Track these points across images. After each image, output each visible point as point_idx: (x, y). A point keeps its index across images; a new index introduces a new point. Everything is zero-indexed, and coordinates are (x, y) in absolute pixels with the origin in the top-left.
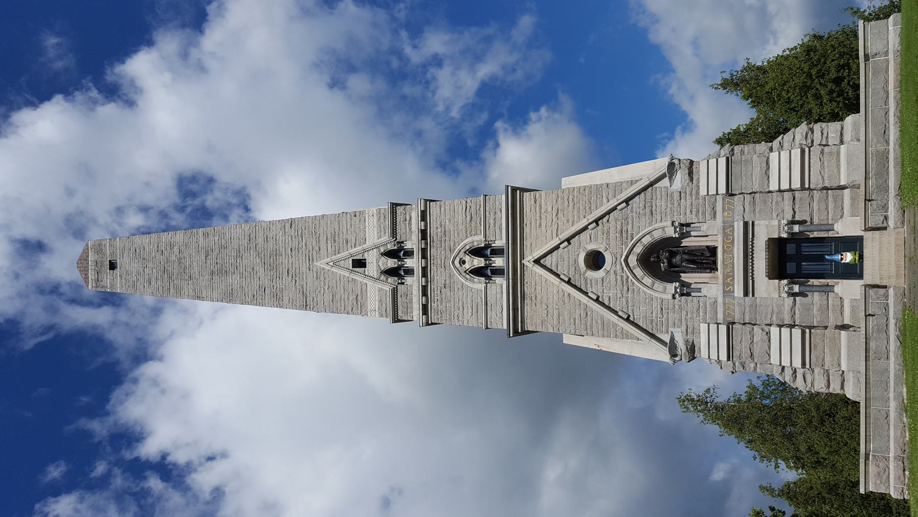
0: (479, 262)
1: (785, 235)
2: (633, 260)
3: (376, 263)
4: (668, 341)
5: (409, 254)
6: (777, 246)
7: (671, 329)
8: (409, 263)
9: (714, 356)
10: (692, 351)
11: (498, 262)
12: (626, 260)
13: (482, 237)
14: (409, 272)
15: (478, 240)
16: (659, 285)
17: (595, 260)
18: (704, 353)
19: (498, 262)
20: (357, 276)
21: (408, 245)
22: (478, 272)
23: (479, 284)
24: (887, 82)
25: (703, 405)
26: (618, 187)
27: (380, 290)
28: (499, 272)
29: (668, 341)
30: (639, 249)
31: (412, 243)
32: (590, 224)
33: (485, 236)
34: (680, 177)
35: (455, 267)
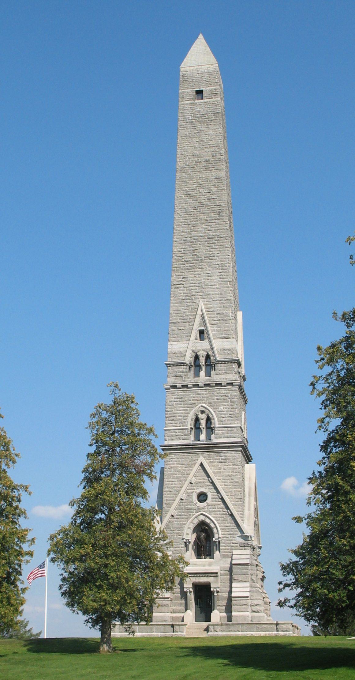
1: (212, 589)
3: (202, 347)
5: (208, 374)
6: (207, 586)
11: (203, 437)
12: (202, 514)
13: (217, 426)
14: (197, 375)
15: (216, 423)
19: (203, 437)
20: (195, 333)
23: (190, 423)
26: (242, 513)
27: (313, 626)
28: (197, 438)
30: (208, 521)
31: (216, 377)
32: (230, 511)
33: (217, 428)
34: (241, 540)
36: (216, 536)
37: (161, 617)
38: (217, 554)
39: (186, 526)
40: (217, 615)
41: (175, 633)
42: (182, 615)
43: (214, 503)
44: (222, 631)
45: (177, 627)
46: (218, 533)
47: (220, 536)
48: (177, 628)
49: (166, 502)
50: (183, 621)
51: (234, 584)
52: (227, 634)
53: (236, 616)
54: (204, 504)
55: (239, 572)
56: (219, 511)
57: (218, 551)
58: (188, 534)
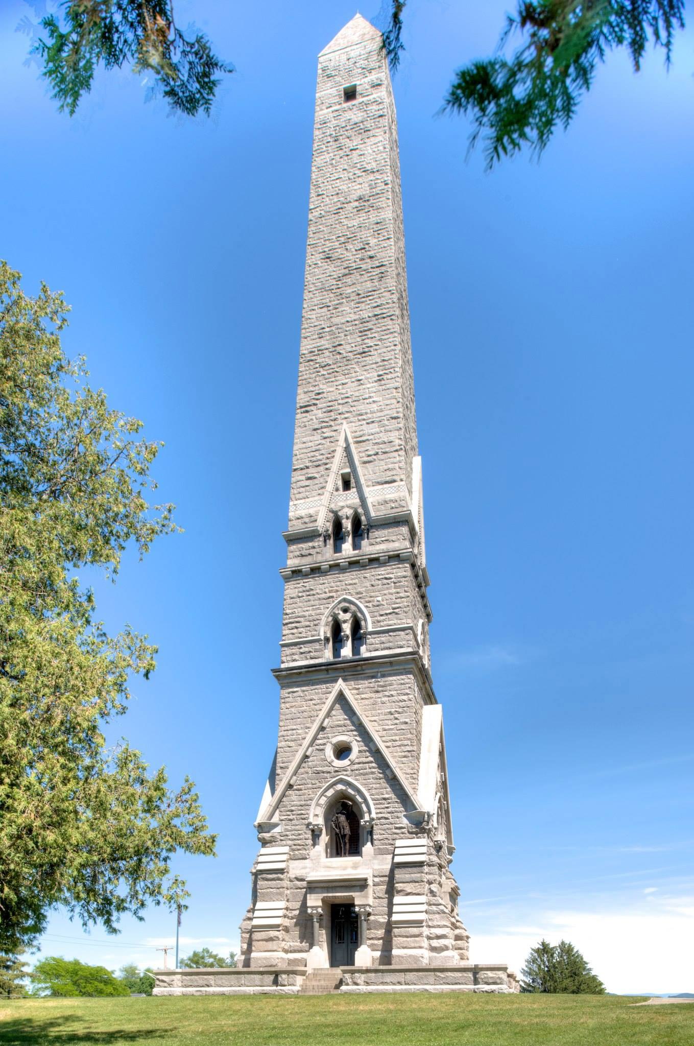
0: (347, 629)
2: (340, 787)
4: (272, 821)
7: (140, 897)
8: (347, 546)
9: (261, 859)
10: (264, 843)
14: (337, 549)
15: (369, 626)
16: (320, 811)
17: (342, 751)
18: (264, 851)
21: (365, 543)
22: (337, 628)
23: (324, 631)
24: (462, 984)
25: (393, 76)
29: (272, 821)
31: (369, 548)
35: (340, 602)
37: (265, 959)
38: (367, 848)
39: (313, 803)
40: (365, 956)
44: (367, 983)
45: (284, 976)
46: (370, 812)
47: (374, 815)
49: (282, 765)
53: (398, 956)
54: (346, 762)
55: (407, 877)
56: (373, 773)
57: (369, 844)
58: (317, 815)
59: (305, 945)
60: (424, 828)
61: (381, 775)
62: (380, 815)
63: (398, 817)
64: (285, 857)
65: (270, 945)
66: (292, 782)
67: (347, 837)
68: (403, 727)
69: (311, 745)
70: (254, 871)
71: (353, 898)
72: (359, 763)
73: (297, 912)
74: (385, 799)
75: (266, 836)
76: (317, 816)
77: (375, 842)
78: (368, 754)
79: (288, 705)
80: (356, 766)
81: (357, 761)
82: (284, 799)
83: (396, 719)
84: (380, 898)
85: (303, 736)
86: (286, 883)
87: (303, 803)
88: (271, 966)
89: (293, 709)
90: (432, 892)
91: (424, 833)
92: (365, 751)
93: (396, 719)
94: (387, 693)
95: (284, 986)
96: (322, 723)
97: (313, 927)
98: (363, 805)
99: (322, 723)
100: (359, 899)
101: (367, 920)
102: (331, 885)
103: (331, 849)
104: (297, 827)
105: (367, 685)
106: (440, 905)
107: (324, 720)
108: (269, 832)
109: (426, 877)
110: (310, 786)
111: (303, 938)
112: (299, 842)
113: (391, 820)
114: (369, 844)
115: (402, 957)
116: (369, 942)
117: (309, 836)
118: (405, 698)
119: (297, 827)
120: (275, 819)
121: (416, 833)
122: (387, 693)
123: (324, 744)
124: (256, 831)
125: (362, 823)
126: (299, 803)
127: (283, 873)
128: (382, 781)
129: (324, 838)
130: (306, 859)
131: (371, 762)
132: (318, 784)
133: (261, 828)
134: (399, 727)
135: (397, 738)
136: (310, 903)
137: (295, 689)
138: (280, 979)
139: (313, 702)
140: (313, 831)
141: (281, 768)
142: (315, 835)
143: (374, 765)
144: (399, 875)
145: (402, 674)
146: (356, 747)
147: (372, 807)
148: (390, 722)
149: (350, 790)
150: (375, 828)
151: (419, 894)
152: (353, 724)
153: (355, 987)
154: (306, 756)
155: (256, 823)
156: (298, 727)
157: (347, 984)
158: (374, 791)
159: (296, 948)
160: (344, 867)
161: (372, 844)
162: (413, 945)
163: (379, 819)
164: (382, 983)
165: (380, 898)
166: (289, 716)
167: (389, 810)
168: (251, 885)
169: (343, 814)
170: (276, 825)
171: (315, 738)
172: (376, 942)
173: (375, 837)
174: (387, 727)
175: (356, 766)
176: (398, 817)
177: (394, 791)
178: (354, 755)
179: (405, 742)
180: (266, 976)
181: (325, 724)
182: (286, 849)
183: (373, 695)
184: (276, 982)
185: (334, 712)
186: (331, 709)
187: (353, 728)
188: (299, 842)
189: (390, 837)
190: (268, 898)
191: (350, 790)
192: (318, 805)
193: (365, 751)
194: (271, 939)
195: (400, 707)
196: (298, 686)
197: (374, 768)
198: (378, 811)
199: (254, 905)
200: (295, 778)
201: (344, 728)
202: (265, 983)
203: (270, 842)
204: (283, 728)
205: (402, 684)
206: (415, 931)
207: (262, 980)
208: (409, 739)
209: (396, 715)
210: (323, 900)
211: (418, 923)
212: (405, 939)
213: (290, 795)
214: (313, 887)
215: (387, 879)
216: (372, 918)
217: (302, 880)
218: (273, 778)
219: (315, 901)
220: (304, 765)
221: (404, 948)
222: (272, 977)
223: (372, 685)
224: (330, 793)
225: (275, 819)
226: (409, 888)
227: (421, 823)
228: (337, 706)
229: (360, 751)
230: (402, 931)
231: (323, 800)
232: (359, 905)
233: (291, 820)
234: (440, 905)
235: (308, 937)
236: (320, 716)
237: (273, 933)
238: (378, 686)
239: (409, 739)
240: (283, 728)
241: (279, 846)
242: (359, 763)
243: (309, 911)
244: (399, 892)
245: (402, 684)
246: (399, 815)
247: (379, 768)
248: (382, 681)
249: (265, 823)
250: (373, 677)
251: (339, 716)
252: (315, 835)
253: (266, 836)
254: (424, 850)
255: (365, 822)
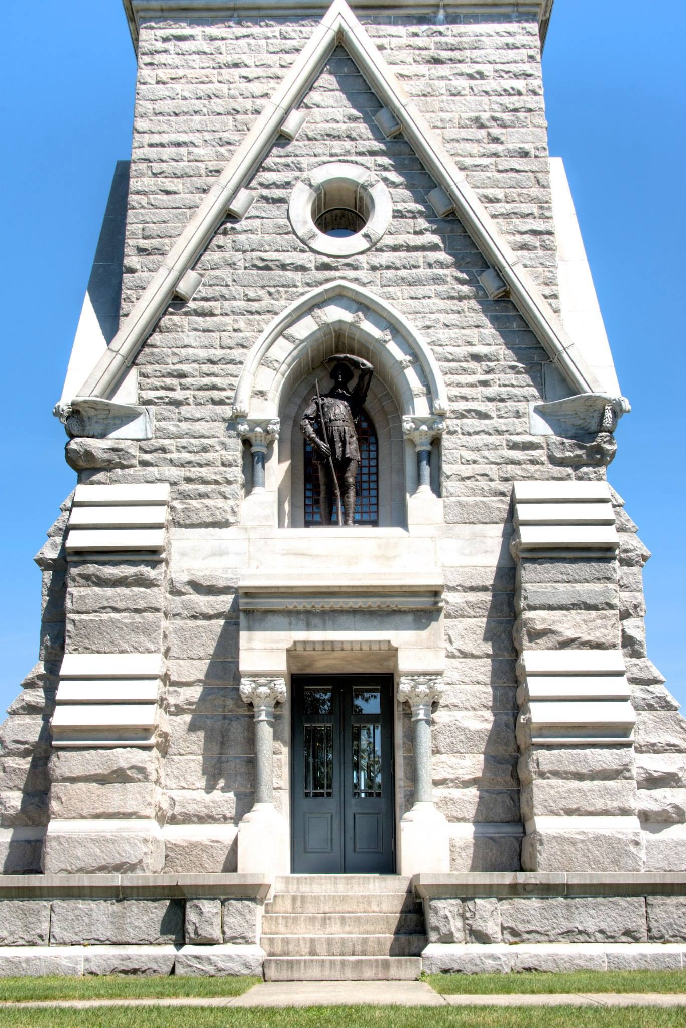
2: (334, 313)
9: (79, 516)
10: (85, 467)
16: (273, 383)
18: (84, 492)
36: (420, 408)
37: (100, 841)
38: (421, 502)
39: (251, 356)
40: (435, 837)
41: (189, 950)
42: (224, 833)
43: (400, 239)
44: (515, 935)
45: (210, 907)
46: (430, 392)
47: (442, 403)
48: (204, 915)
49: (144, 244)
50: (231, 866)
51: (533, 658)
52: (656, 958)
53: (559, 839)
54: (354, 243)
55: (564, 592)
56: (438, 280)
57: (425, 489)
58: (261, 393)
59: (224, 799)
60: (599, 450)
61: (465, 289)
62: (461, 406)
63: (518, 415)
64: (160, 515)
65: (116, 796)
66: (183, 288)
67: (353, 466)
68: (516, 163)
69: (246, 181)
70: (52, 554)
71: (392, 652)
72: (395, 249)
73: (195, 693)
74: (476, 358)
75: (97, 446)
76: (260, 390)
77: (449, 485)
78: (422, 223)
79: (164, 74)
80: (385, 258)
81: (389, 241)
82: (156, 338)
83: (496, 140)
84: (465, 655)
85: (212, 165)
86: (159, 597)
87: (219, 353)
88: (119, 868)
89: (178, 87)
90: (628, 641)
91: (598, 464)
92: (414, 215)
93: (496, 140)
94: (463, 68)
95: (211, 943)
96: (282, 120)
97: (251, 741)
98: (411, 375)
99: (282, 120)
100: (415, 653)
101: (431, 722)
102: (320, 604)
103: (293, 506)
104: (199, 427)
105: (405, 41)
106: (656, 681)
107: (287, 112)
108: (103, 436)
109: (622, 598)
110: (241, 304)
111: (214, 773)
112: (204, 472)
113: (500, 424)
114: (425, 489)
115: (573, 843)
116: (441, 791)
117: (235, 452)
118: (520, 84)
119: (199, 427)
120: (126, 396)
121: (576, 464)
122: (463, 68)
123: (287, 185)
124: (60, 426)
125: (407, 426)
126: (203, 354)
127: (154, 564)
128: (464, 304)
129: (276, 471)
130: (225, 524)
131: (434, 248)
132: (266, 302)
133: (78, 419)
134: (504, 163)
135: (499, 193)
136: (247, 662)
137: (187, 31)
138: (192, 915)
139: (244, 72)
140: (247, 443)
141: (141, 251)
142: (253, 458)
143: (442, 256)
144: (536, 582)
145: (507, 18)
146: (387, 201)
147: (440, 380)
148: (474, 148)
149: (367, 326)
150: (447, 441)
151: (599, 646)
152: (378, 134)
153: (477, 949)
154: (229, 215)
155: (64, 403)
156: (195, 137)
157: (448, 939)
158: (443, 334)
159: (191, 809)
160: (344, 554)
161: (437, 490)
162: (600, 804)
163: (461, 416)
164: (570, 934)
165: (465, 655)
166: (166, 106)
167: (491, 391)
168: (39, 602)
169: (342, 397)
170: (127, 415)
171: (258, 165)
172: (456, 793)
173: (446, 468)
174: (468, 161)
175: (385, 258)
176: (518, 415)
177: (505, 333)
178: (379, 221)
179: (525, 208)
180: (134, 906)
181: (289, 126)
182: (162, 492)
183: (423, 69)
184: (176, 928)
185: (314, 97)
186: (309, 86)
187: (377, 145)
188: (204, 472)
189: (493, 471)
190: (99, 641)
191: (367, 326)
192: (265, 362)
193: (414, 215)
194: (120, 776)
195: (506, 110)
196: (193, 22)
197: (442, 265)
198: (456, 391)
199: (53, 661)
200: (192, 275)
201: (348, 144)
202: (131, 934)
203: (109, 466)
204: (147, 139)
205: (508, 46)
206: (606, 758)
207: (118, 922)
208: (533, 200)
209: (496, 131)
210: (291, 653)
211: (615, 735)
212: (574, 784)
213: (175, 328)
214: (252, 608)
215: (487, 597)
216: (441, 716)
217: (212, 590)
218: (108, 291)
219: (265, 655)
220: (220, 240)
221: (569, 812)
222: (158, 910)
223: (418, 42)
224: (305, 328)
225: (126, 396)
226: (568, 624)
227: (593, 435)
228: (327, 79)
229: (398, 215)
230: (566, 758)
231: (283, 351)
232: (412, 674)
233: (177, 403)
234: (656, 681)
235: (232, 766)
236: (276, 98)
237: (125, 757)
238: (440, 46)
239: (533, 200)
240: (147, 139)
241: (136, 480)
242: (395, 249)
243: (246, 686)
244: (536, 635)
245: (508, 46)
246: (522, 406)
247: (458, 265)
248: (452, 32)
249: (93, 405)
250: (422, 20)
251: (332, 104)
252: (253, 458)
253: (97, 446)
254: (605, 512)
255: (418, 422)
